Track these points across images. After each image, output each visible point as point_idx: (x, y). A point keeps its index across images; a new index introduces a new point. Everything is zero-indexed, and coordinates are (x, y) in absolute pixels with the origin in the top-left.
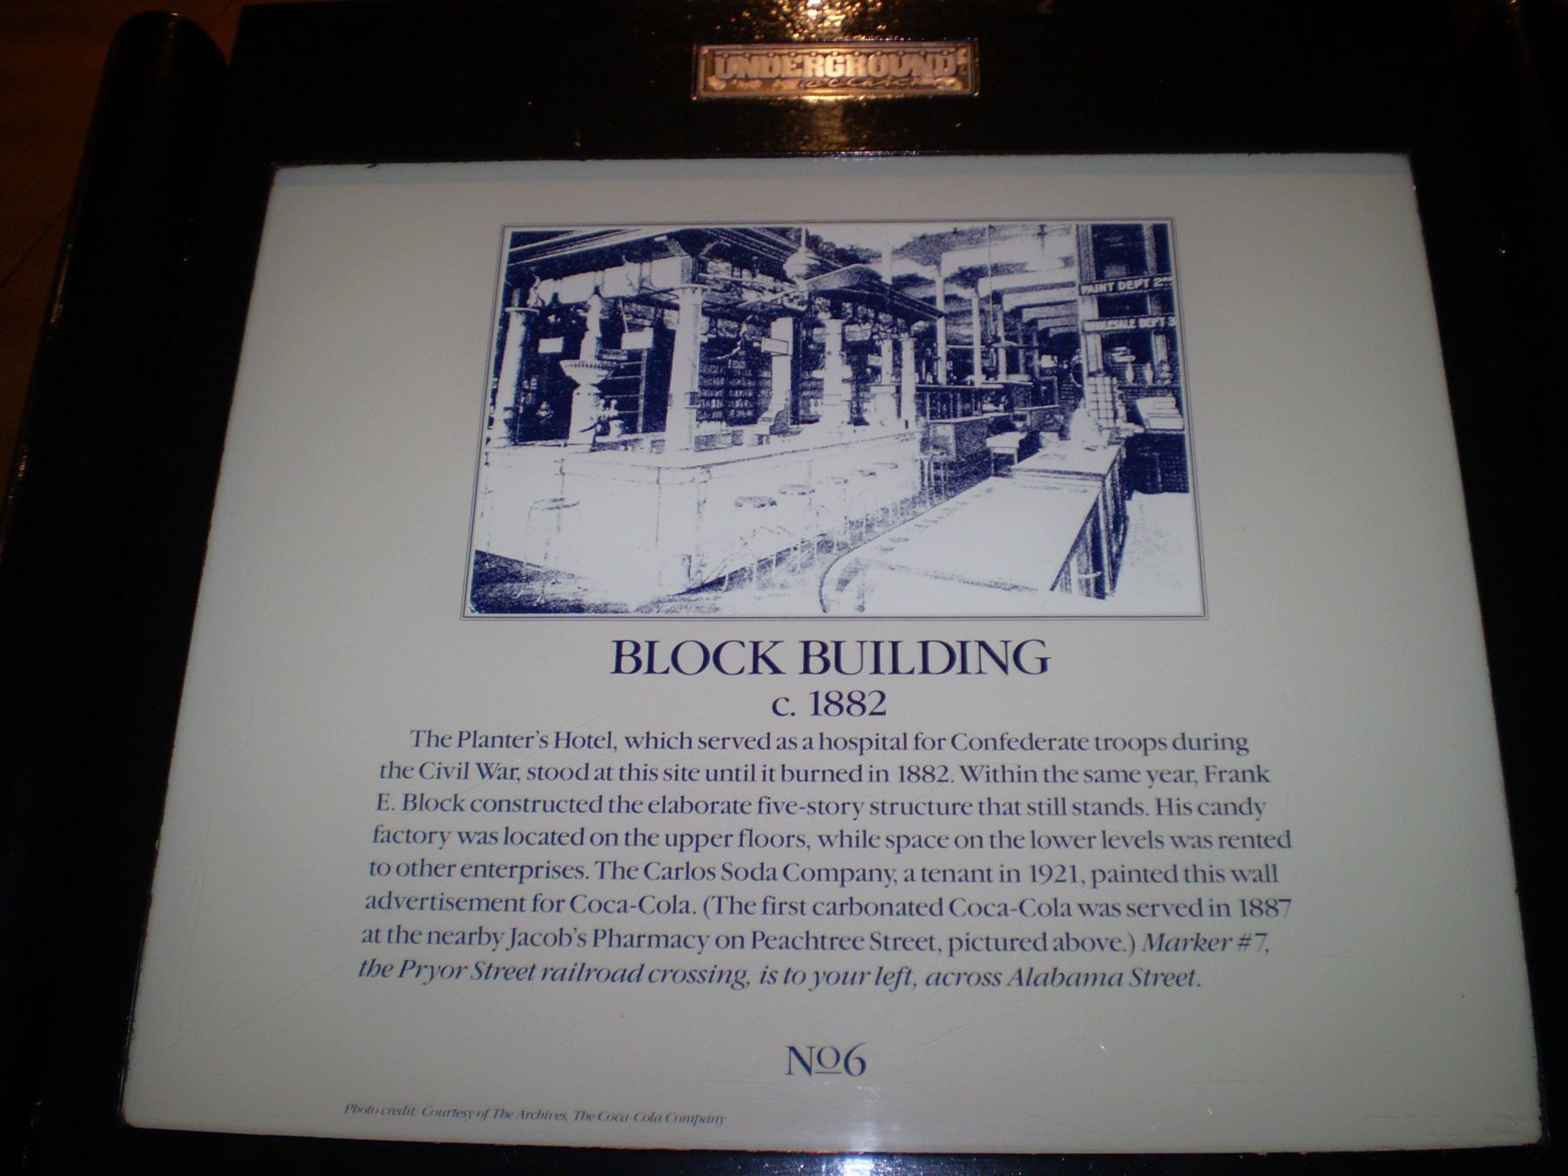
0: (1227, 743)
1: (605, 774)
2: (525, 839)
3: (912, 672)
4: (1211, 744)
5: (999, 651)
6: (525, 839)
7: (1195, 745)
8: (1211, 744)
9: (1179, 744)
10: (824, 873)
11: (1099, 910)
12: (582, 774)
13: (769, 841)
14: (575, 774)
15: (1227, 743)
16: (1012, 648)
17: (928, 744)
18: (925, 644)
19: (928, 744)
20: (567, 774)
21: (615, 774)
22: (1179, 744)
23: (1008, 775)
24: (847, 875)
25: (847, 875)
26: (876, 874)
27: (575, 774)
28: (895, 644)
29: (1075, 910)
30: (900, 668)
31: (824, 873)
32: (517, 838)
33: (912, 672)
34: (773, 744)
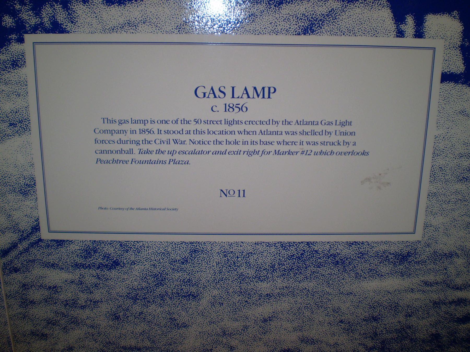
0: (134, 142)
1: (188, 132)
2: (214, 133)
3: (238, 98)
4: (129, 142)
5: (225, 192)
6: (214, 133)
7: (124, 142)
8: (129, 142)
9: (119, 142)
10: (106, 131)
11: (291, 133)
12: (181, 132)
13: (174, 132)
14: (179, 132)
15: (134, 142)
16: (228, 191)
17: (99, 142)
18: (244, 196)
19: (99, 142)
20: (176, 132)
21: (192, 132)
22: (119, 142)
23: (198, 132)
24: (113, 132)
25: (113, 132)
26: (122, 131)
27: (179, 132)
28: (239, 196)
29: (284, 133)
30: (235, 96)
31: (106, 131)
32: (211, 133)
33: (238, 98)
34: (184, 132)
